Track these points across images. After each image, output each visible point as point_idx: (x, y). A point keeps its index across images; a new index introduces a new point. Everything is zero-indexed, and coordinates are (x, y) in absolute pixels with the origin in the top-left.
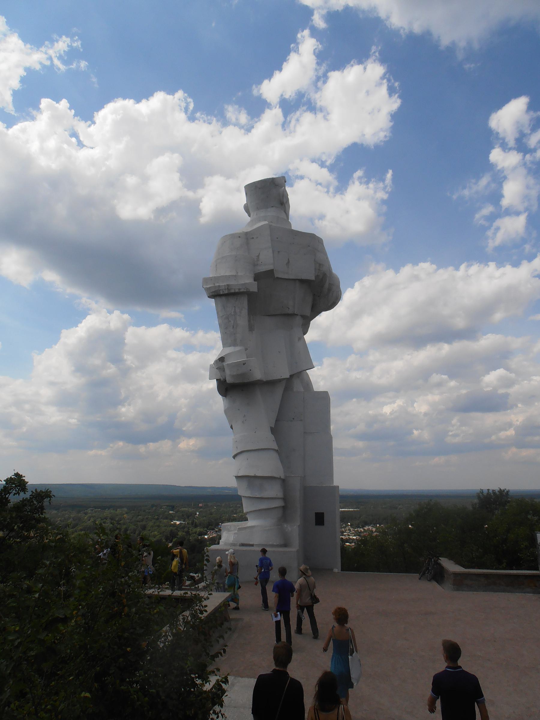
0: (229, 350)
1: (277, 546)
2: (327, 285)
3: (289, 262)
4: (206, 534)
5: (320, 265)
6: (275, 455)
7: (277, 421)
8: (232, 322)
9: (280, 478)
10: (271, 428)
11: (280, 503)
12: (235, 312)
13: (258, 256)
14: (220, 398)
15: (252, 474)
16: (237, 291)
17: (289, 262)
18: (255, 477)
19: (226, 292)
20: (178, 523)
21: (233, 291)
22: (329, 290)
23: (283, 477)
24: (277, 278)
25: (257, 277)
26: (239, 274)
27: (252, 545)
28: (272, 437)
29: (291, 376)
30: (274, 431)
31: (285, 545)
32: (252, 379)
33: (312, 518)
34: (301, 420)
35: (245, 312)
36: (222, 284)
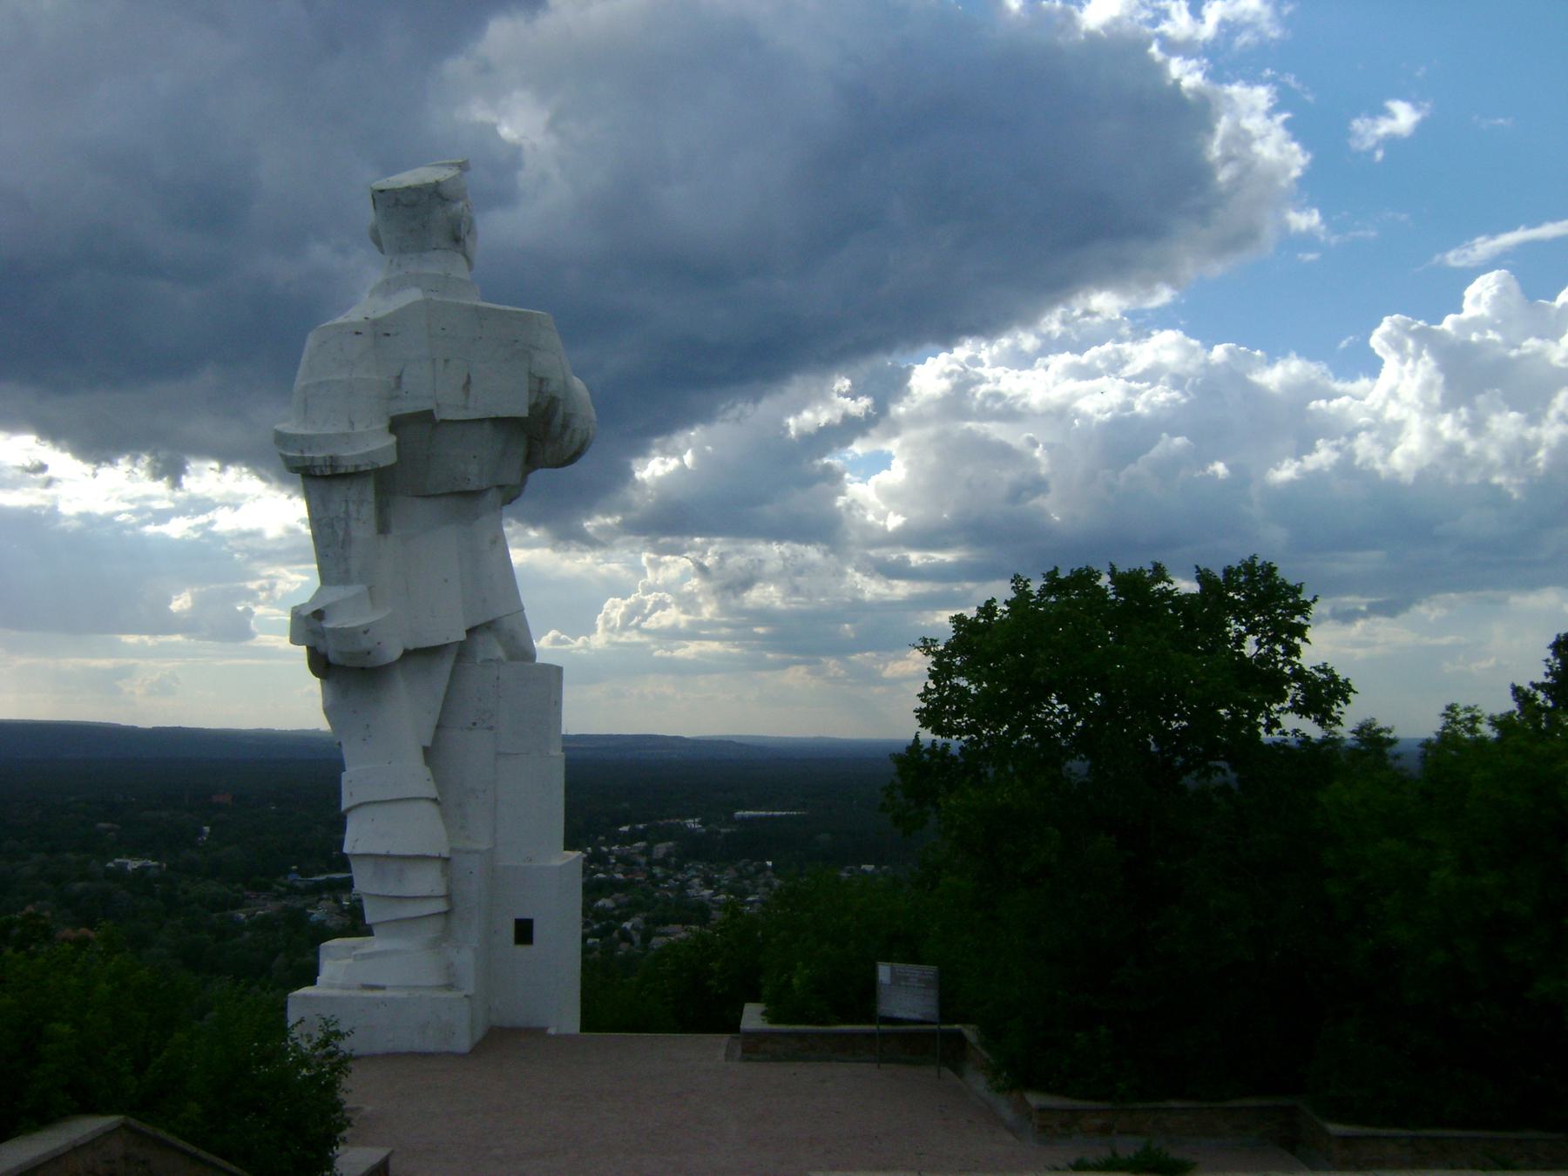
0: (339, 593)
1: (439, 987)
2: (558, 420)
3: (468, 382)
4: (238, 904)
5: (541, 380)
6: (433, 809)
7: (438, 727)
8: (341, 533)
9: (439, 857)
10: (426, 750)
11: (441, 906)
12: (347, 512)
13: (399, 378)
14: (315, 684)
15: (383, 851)
16: (351, 470)
17: (468, 382)
18: (388, 856)
19: (328, 472)
20: (133, 864)
21: (342, 471)
22: (565, 426)
23: (445, 854)
24: (443, 421)
25: (397, 425)
26: (359, 428)
27: (383, 988)
28: (427, 772)
29: (471, 631)
30: (429, 754)
31: (449, 986)
32: (382, 662)
33: (509, 931)
34: (491, 728)
35: (369, 511)
36: (319, 454)
